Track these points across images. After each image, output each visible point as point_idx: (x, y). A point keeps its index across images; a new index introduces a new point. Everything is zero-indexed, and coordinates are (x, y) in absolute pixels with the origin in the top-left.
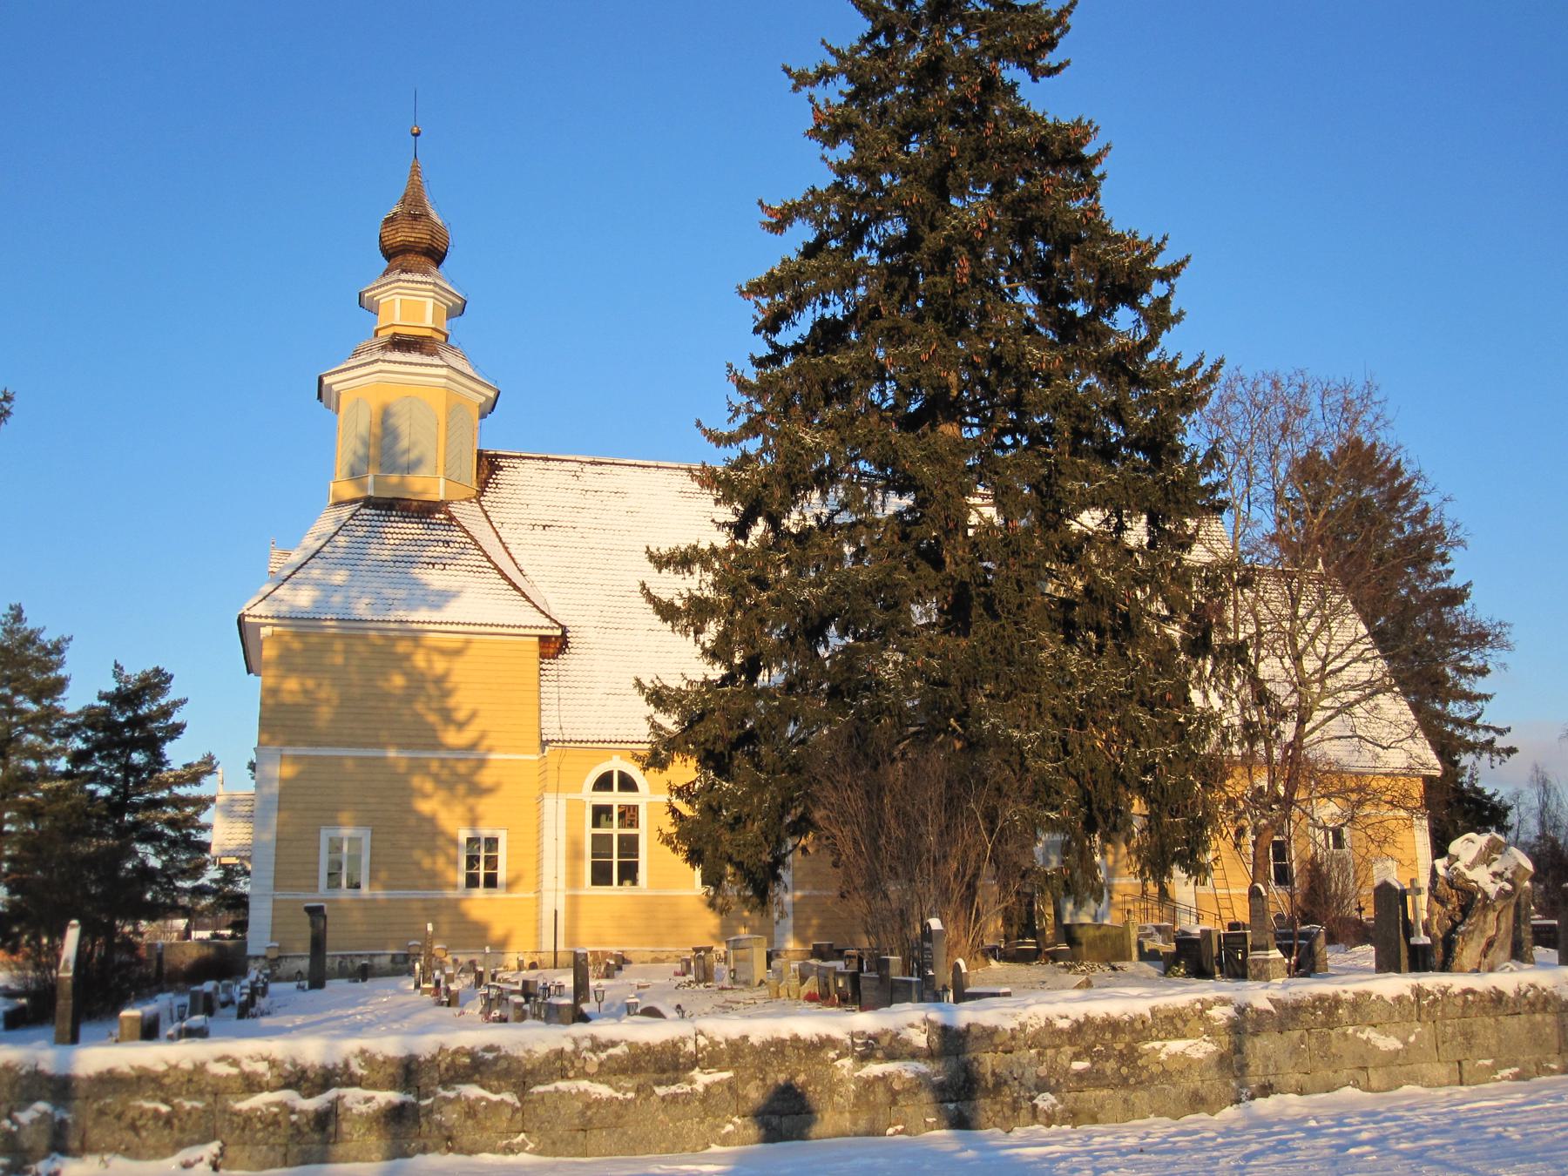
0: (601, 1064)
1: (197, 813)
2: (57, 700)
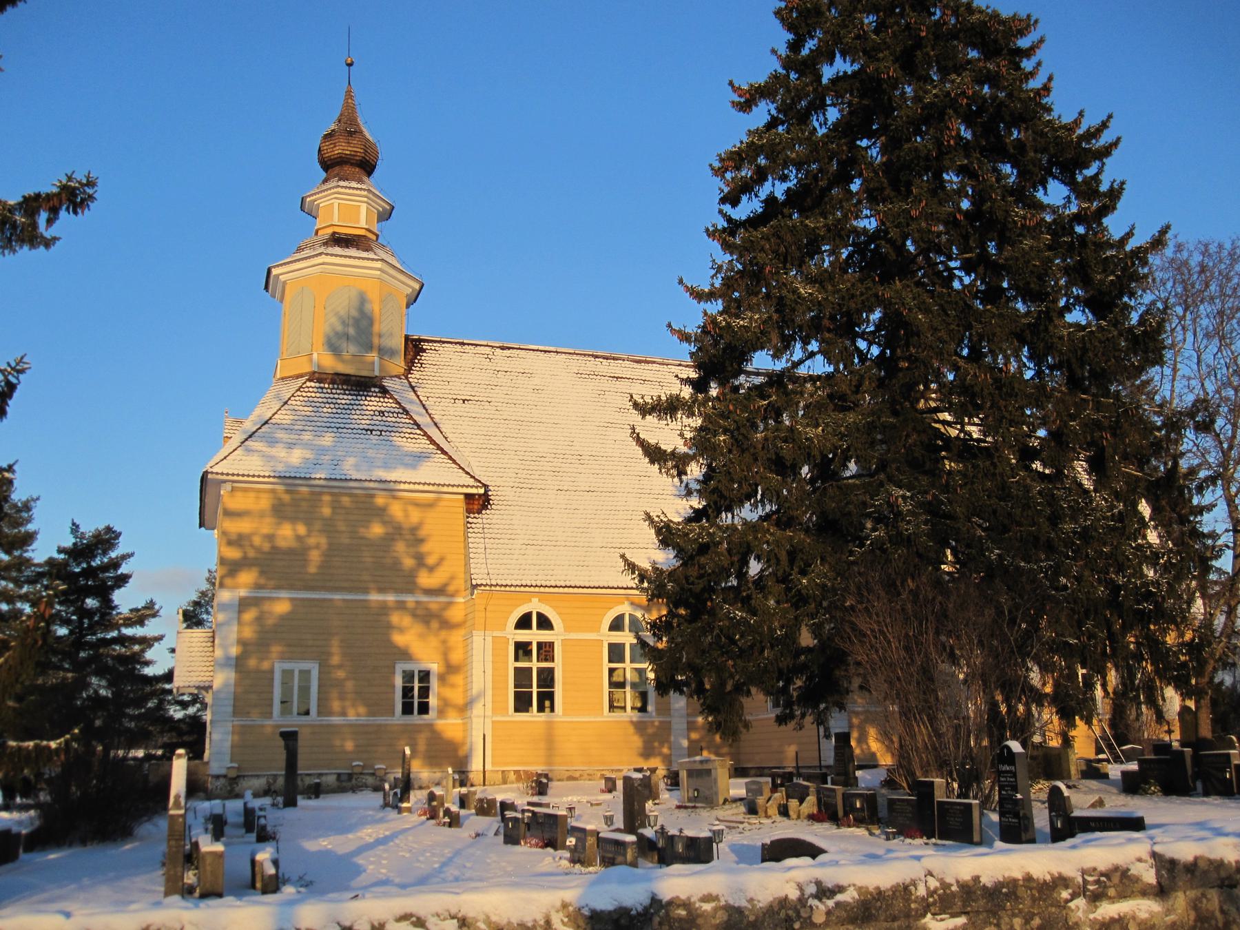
0: (829, 913)
1: (143, 651)
2: (27, 551)
